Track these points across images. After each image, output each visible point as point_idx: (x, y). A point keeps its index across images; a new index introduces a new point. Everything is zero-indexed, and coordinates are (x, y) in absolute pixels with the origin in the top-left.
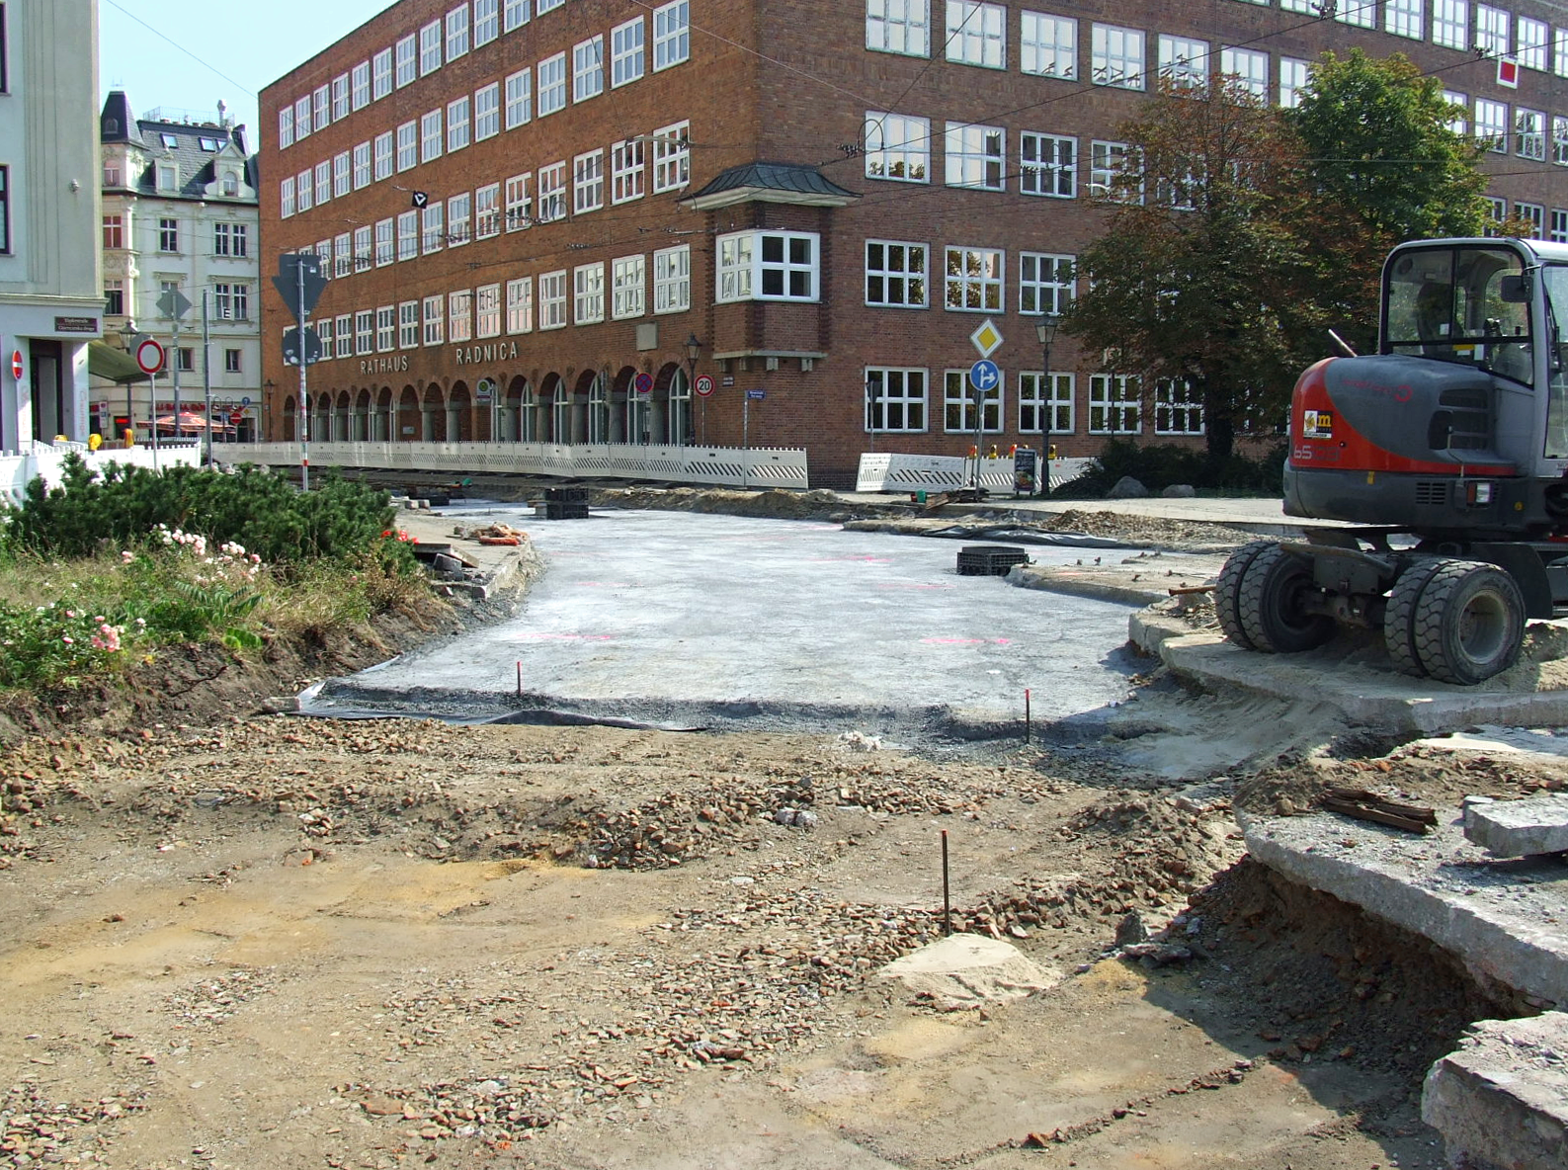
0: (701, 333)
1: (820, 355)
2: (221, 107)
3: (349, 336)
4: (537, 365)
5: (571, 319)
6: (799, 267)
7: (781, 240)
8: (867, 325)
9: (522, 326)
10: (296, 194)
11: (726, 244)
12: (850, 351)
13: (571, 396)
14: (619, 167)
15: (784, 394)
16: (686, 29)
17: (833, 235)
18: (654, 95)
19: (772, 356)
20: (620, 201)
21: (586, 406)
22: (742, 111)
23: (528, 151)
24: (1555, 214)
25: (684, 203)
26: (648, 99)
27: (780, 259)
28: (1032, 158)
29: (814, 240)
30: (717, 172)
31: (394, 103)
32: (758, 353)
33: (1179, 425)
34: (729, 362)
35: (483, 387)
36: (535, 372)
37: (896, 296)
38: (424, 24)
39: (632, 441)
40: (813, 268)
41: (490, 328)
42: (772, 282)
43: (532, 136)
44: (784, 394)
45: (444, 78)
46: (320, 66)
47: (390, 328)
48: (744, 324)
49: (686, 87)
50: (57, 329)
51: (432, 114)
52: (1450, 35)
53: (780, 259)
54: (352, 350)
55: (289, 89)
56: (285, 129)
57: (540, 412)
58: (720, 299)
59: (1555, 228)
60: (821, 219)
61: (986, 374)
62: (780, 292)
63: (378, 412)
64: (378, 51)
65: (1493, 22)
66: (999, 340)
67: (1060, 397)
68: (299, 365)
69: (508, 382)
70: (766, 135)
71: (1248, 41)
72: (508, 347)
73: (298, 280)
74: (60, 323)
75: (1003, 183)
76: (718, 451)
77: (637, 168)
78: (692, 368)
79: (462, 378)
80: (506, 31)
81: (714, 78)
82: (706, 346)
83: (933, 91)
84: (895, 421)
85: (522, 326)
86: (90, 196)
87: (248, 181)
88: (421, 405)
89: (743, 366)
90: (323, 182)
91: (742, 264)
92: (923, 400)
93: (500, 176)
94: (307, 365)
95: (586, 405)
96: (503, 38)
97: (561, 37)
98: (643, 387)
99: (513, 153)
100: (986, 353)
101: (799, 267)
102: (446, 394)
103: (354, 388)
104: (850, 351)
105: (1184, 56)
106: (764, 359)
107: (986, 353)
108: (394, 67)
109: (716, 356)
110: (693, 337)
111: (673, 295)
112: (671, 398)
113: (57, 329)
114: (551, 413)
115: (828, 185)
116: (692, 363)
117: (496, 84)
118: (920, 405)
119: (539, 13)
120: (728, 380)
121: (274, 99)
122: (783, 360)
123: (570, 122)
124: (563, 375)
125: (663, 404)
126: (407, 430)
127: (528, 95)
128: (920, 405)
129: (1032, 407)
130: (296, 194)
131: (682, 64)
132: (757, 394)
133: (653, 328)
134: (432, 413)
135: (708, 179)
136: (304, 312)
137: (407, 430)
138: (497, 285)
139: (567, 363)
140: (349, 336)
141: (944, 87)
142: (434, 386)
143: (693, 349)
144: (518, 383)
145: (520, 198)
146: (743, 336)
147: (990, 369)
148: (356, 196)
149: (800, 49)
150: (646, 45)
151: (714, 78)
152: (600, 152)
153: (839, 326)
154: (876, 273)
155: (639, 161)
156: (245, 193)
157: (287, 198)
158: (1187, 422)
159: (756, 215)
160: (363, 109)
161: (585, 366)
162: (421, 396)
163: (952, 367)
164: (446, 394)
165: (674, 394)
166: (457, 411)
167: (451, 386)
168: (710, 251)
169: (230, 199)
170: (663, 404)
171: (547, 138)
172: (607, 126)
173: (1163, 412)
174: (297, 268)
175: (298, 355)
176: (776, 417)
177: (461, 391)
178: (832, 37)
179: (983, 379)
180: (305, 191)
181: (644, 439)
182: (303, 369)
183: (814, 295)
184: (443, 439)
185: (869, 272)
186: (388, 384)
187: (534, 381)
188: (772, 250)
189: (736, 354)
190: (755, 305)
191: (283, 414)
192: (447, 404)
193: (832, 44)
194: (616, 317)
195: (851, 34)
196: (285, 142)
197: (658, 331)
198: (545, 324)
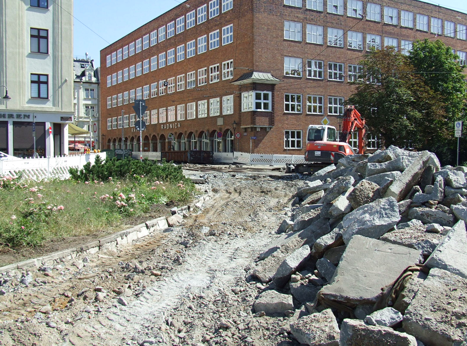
0: (237, 120)
2: (86, 55)
4: (186, 130)
5: (186, 118)
6: (258, 101)
9: (172, 119)
10: (111, 80)
11: (244, 94)
12: (280, 125)
13: (197, 138)
14: (212, 73)
16: (232, 34)
17: (275, 92)
18: (221, 53)
20: (212, 82)
21: (213, 141)
23: (184, 68)
26: (221, 53)
29: (270, 93)
30: (242, 74)
31: (142, 54)
34: (245, 128)
35: (170, 136)
36: (186, 132)
38: (151, 32)
40: (270, 102)
41: (171, 119)
42: (258, 106)
43: (185, 64)
46: (119, 43)
48: (250, 118)
50: (61, 120)
51: (154, 57)
55: (110, 50)
56: (108, 61)
58: (243, 111)
62: (289, 111)
64: (137, 39)
67: (294, 141)
68: (140, 131)
69: (177, 134)
72: (178, 124)
73: (139, 107)
74: (62, 118)
78: (235, 130)
80: (177, 34)
81: (241, 47)
82: (238, 124)
84: (293, 145)
85: (172, 119)
86: (71, 83)
87: (95, 76)
88: (150, 141)
89: (250, 130)
90: (120, 77)
93: (175, 75)
95: (213, 141)
97: (194, 35)
98: (219, 136)
101: (258, 101)
102: (158, 138)
106: (256, 128)
108: (142, 44)
109: (242, 127)
110: (235, 121)
111: (229, 109)
112: (227, 139)
113: (61, 120)
114: (190, 144)
116: (234, 129)
117: (174, 49)
118: (300, 141)
119: (187, 29)
122: (261, 128)
123: (197, 60)
124: (194, 133)
125: (225, 141)
126: (145, 148)
128: (300, 141)
130: (111, 80)
131: (231, 43)
133: (222, 119)
134: (154, 143)
135: (239, 77)
136: (141, 116)
137: (145, 148)
138: (174, 107)
139: (195, 129)
142: (154, 136)
143: (235, 125)
144: (181, 134)
151: (241, 47)
152: (206, 68)
154: (287, 103)
156: (94, 79)
157: (109, 81)
158: (376, 144)
160: (133, 56)
161: (201, 130)
162: (150, 139)
164: (158, 138)
166: (161, 143)
168: (240, 97)
169: (90, 81)
170: (225, 141)
174: (139, 103)
175: (139, 127)
177: (163, 137)
178: (274, 36)
180: (115, 79)
182: (141, 131)
183: (270, 110)
184: (157, 151)
185: (285, 103)
187: (186, 134)
188: (258, 97)
189: (248, 126)
190: (254, 112)
191: (107, 144)
194: (211, 116)
196: (108, 65)
198: (179, 119)
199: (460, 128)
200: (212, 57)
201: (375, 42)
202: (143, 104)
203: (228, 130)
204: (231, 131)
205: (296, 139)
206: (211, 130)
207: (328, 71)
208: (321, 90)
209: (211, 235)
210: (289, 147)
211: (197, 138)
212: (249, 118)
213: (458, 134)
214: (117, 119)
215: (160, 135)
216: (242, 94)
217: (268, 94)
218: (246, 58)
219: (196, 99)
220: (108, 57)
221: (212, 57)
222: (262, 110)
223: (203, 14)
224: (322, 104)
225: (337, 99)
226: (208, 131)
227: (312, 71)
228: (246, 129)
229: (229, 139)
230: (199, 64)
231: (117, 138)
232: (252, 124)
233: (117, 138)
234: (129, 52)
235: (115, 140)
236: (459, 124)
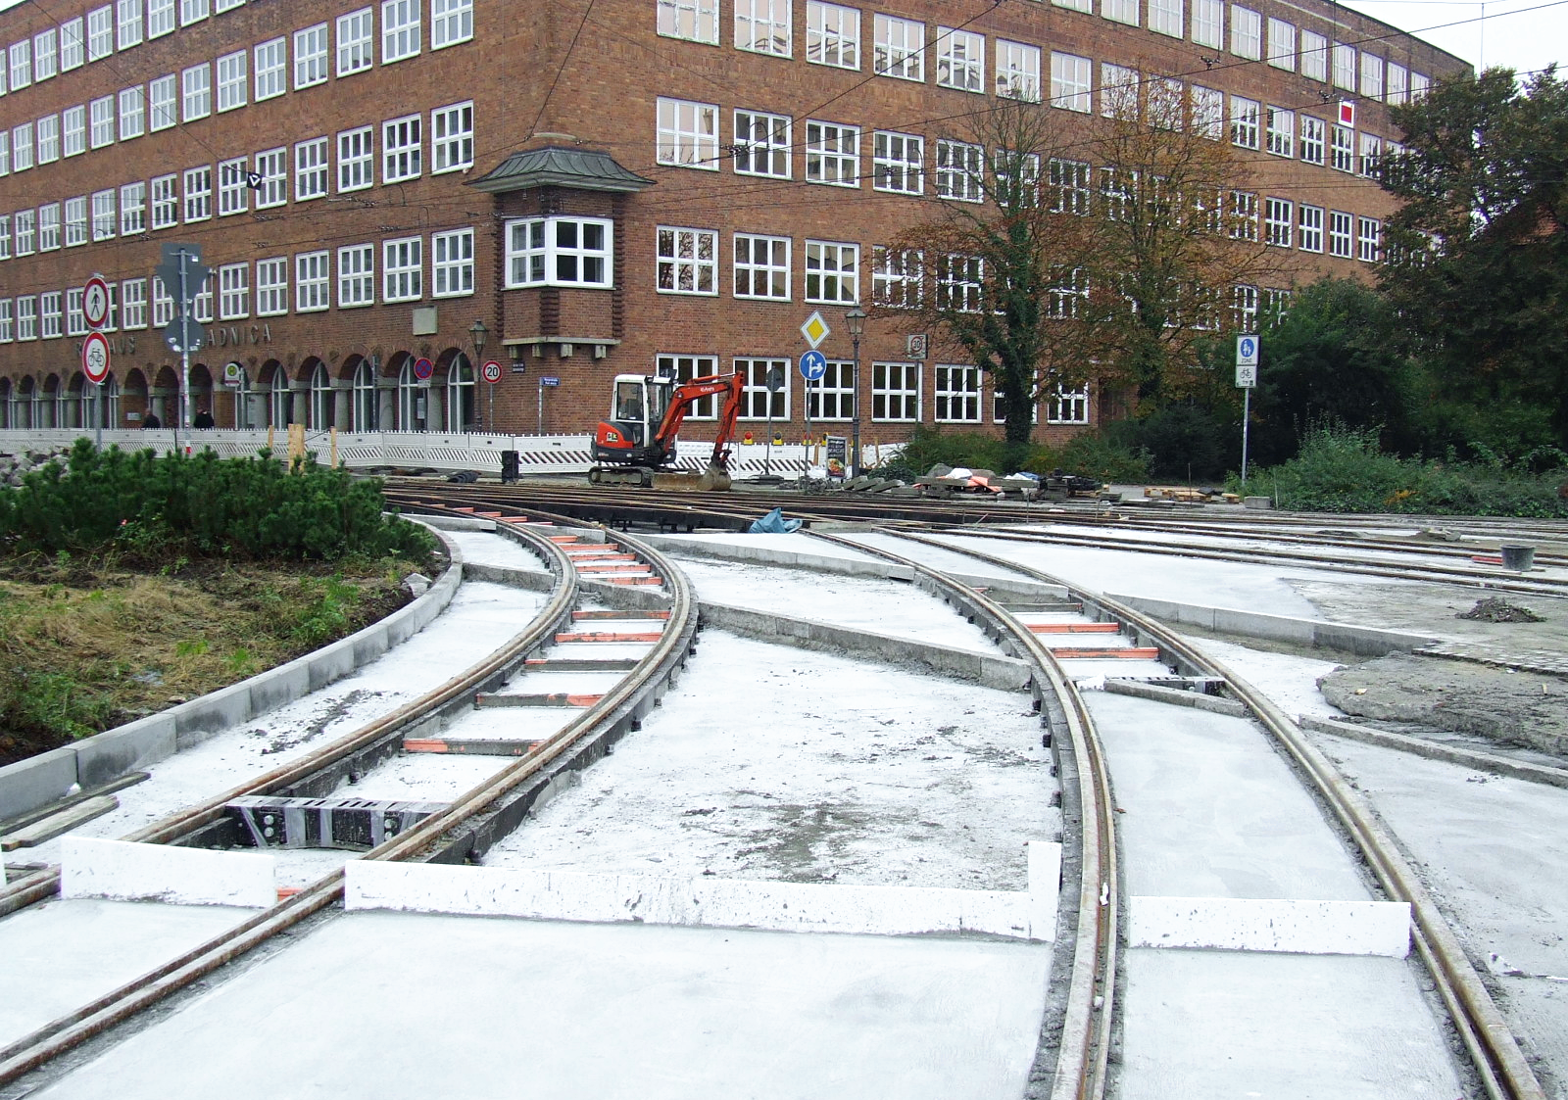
1: (613, 342)
4: (294, 349)
6: (567, 251)
12: (642, 338)
15: (577, 381)
19: (567, 342)
22: (533, 94)
23: (283, 125)
24: (1302, 210)
27: (574, 245)
28: (884, 156)
29: (608, 226)
32: (552, 339)
36: (292, 357)
37: (761, 288)
39: (405, 428)
40: (606, 253)
42: (566, 267)
43: (287, 109)
44: (577, 381)
45: (179, 44)
49: (471, 66)
52: (1207, 34)
53: (574, 245)
57: (297, 400)
58: (510, 284)
59: (1302, 223)
60: (617, 204)
61: (814, 364)
62: (574, 278)
64: (94, 8)
65: (1246, 22)
66: (826, 331)
68: (182, 353)
70: (560, 120)
71: (1021, 34)
75: (857, 182)
76: (562, 439)
77: (411, 147)
81: (503, 59)
83: (722, 78)
88: (151, 390)
89: (536, 353)
94: (190, 353)
99: (265, 125)
100: (814, 345)
101: (567, 251)
102: (151, 380)
104: (642, 338)
105: (964, 52)
106: (558, 345)
107: (814, 345)
108: (115, 26)
109: (506, 342)
120: (517, 368)
122: (577, 347)
126: (131, 416)
129: (834, 395)
132: (551, 381)
137: (131, 416)
139: (329, 347)
141: (733, 74)
147: (818, 359)
148: (67, 164)
151: (503, 59)
153: (631, 313)
155: (415, 140)
161: (353, 350)
163: (741, 355)
171: (306, 111)
172: (377, 102)
175: (180, 343)
176: (570, 404)
178: (625, 22)
179: (811, 369)
181: (420, 426)
182: (186, 357)
183: (608, 282)
185: (660, 259)
188: (566, 236)
193: (625, 29)
195: (643, 19)
199: (1254, 358)
200: (393, 87)
201: (962, 56)
202: (195, 260)
203: (454, 351)
205: (822, 390)
206: (391, 349)
207: (808, 150)
208: (784, 217)
209: (699, 618)
211: (334, 382)
213: (1246, 375)
215: (71, 375)
217: (600, 228)
218: (521, 99)
219: (333, 239)
221: (393, 87)
222: (580, 282)
224: (783, 264)
225: (765, 244)
227: (752, 149)
229: (320, 388)
230: (343, 112)
231: (65, 372)
233: (15, 375)
234: (58, 55)
235: (52, 383)
236: (1250, 344)
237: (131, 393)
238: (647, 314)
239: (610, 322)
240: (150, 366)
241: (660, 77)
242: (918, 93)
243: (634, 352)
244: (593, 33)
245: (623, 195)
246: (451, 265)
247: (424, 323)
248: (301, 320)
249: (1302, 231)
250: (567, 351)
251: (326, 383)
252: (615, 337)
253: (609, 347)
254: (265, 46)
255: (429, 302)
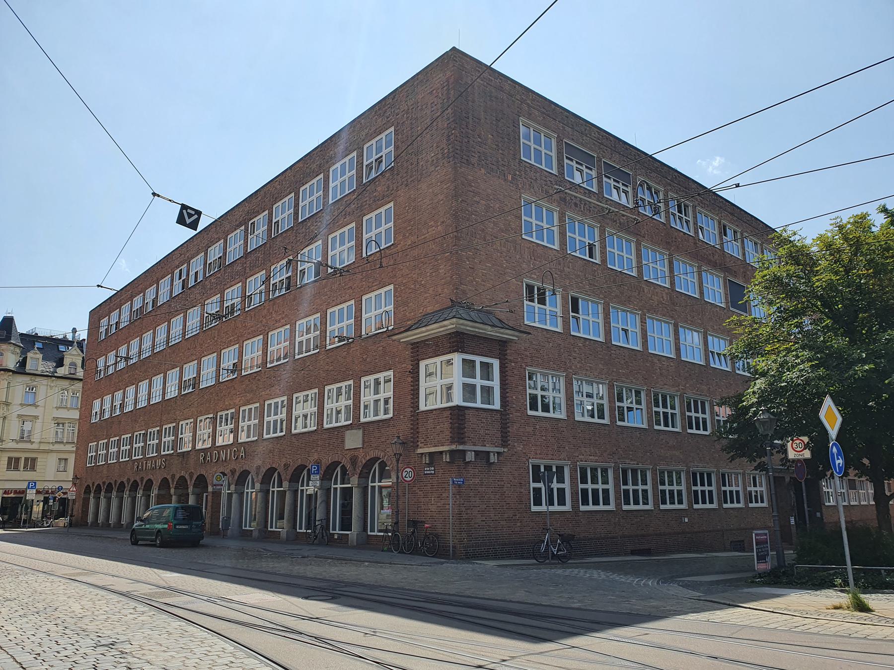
1: (501, 450)
3: (129, 447)
5: (289, 429)
7: (474, 361)
8: (530, 429)
12: (520, 448)
13: (286, 484)
15: (477, 481)
19: (470, 450)
25: (394, 338)
29: (496, 363)
32: (461, 447)
33: (595, 502)
36: (258, 468)
38: (192, 258)
42: (469, 390)
47: (94, 454)
54: (130, 456)
57: (234, 496)
58: (422, 407)
60: (500, 348)
63: (143, 495)
69: (237, 474)
70: (463, 287)
79: (203, 472)
82: (409, 444)
88: (172, 491)
89: (446, 458)
91: (444, 382)
92: (713, 488)
96: (246, 255)
103: (129, 480)
104: (520, 448)
106: (464, 452)
109: (420, 451)
115: (504, 326)
116: (398, 456)
118: (564, 489)
120: (430, 470)
121: (96, 315)
122: (477, 453)
127: (214, 368)
128: (564, 489)
130: (107, 362)
133: (360, 433)
140: (129, 447)
141: (566, 269)
142: (182, 478)
144: (245, 474)
145: (249, 420)
146: (447, 433)
149: (483, 230)
150: (357, 240)
153: (513, 429)
159: (458, 342)
161: (299, 462)
165: (273, 487)
167: (194, 478)
173: (595, 492)
183: (497, 406)
186: (151, 477)
188: (468, 367)
189: (441, 449)
190: (458, 412)
192: (190, 490)
197: (364, 434)
204: (279, 474)
206: (327, 460)
210: (552, 504)
211: (286, 484)
212: (445, 426)
214: (107, 444)
216: (422, 364)
220: (104, 322)
223: (237, 245)
226: (318, 463)
228: (433, 457)
229: (276, 489)
231: (104, 483)
232: (452, 443)
237: (180, 492)
238: (521, 430)
239: (499, 435)
240: (173, 476)
241: (524, 266)
242: (667, 294)
243: (514, 458)
244: (483, 230)
245: (66, 459)
246: (377, 395)
247: (353, 440)
248: (265, 443)
249: (690, 418)
250: (470, 457)
251: (280, 485)
252: (503, 446)
253: (498, 453)
254: (276, 332)
255: (356, 425)
